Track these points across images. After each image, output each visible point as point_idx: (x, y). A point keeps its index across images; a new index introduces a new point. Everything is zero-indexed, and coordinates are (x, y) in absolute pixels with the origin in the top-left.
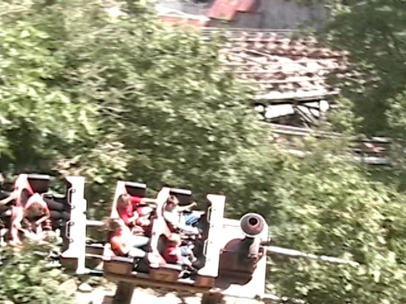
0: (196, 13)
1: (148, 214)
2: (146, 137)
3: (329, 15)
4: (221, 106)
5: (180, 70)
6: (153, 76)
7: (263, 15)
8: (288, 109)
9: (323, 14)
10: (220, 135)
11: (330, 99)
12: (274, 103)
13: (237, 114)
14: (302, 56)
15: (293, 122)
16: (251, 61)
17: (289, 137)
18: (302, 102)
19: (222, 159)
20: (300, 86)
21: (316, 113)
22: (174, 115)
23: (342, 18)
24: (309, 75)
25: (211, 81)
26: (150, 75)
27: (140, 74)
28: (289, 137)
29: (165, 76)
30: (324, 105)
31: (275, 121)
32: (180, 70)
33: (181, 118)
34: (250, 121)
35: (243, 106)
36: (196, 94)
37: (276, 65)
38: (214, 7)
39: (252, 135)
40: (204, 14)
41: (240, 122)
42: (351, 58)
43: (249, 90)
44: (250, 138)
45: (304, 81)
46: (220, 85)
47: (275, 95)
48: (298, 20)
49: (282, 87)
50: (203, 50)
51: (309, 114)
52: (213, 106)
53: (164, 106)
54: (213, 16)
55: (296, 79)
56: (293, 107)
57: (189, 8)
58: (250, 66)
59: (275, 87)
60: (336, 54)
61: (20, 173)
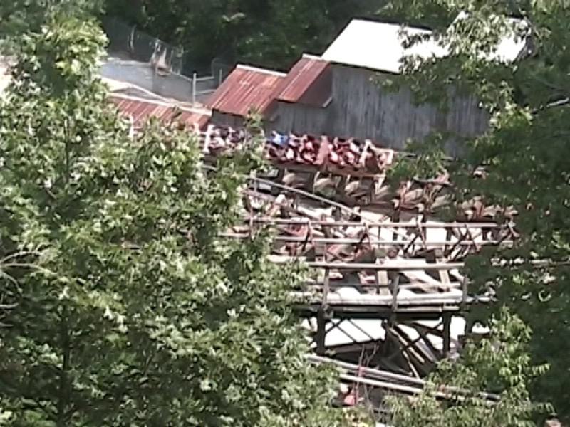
0: (187, 97)
1: (351, 322)
2: (48, 368)
3: (481, 125)
4: (232, 313)
5: (145, 230)
6: (83, 233)
7: (332, 112)
8: (374, 329)
9: (468, 122)
10: (226, 376)
11: (473, 313)
12: (346, 312)
13: (261, 335)
14: (415, 211)
15: (386, 361)
16: (301, 214)
17: (375, 395)
18: (411, 316)
19: (476, 198)
20: (406, 281)
21: (437, 342)
22: (123, 329)
23: (510, 138)
24: (429, 255)
25: (210, 257)
26: (81, 233)
27: (54, 226)
28: (375, 395)
29: (111, 236)
30: (458, 326)
31: (349, 353)
32: (145, 230)
33: (139, 337)
34: (291, 352)
35: (278, 319)
36: (179, 285)
37: (353, 230)
38: (225, 86)
39: (292, 386)
40: (200, 99)
41: (268, 353)
42: (526, 224)
43: (293, 284)
44: (290, 391)
45: (416, 270)
46: (232, 267)
47: (348, 295)
48: (411, 129)
49: (364, 279)
50: (200, 180)
51: (421, 344)
52: (212, 312)
53: (105, 302)
54: (221, 106)
55: (399, 262)
56: (384, 326)
57: (166, 86)
58: (297, 226)
59: (349, 278)
60: (490, 211)
61: (449, 337)
